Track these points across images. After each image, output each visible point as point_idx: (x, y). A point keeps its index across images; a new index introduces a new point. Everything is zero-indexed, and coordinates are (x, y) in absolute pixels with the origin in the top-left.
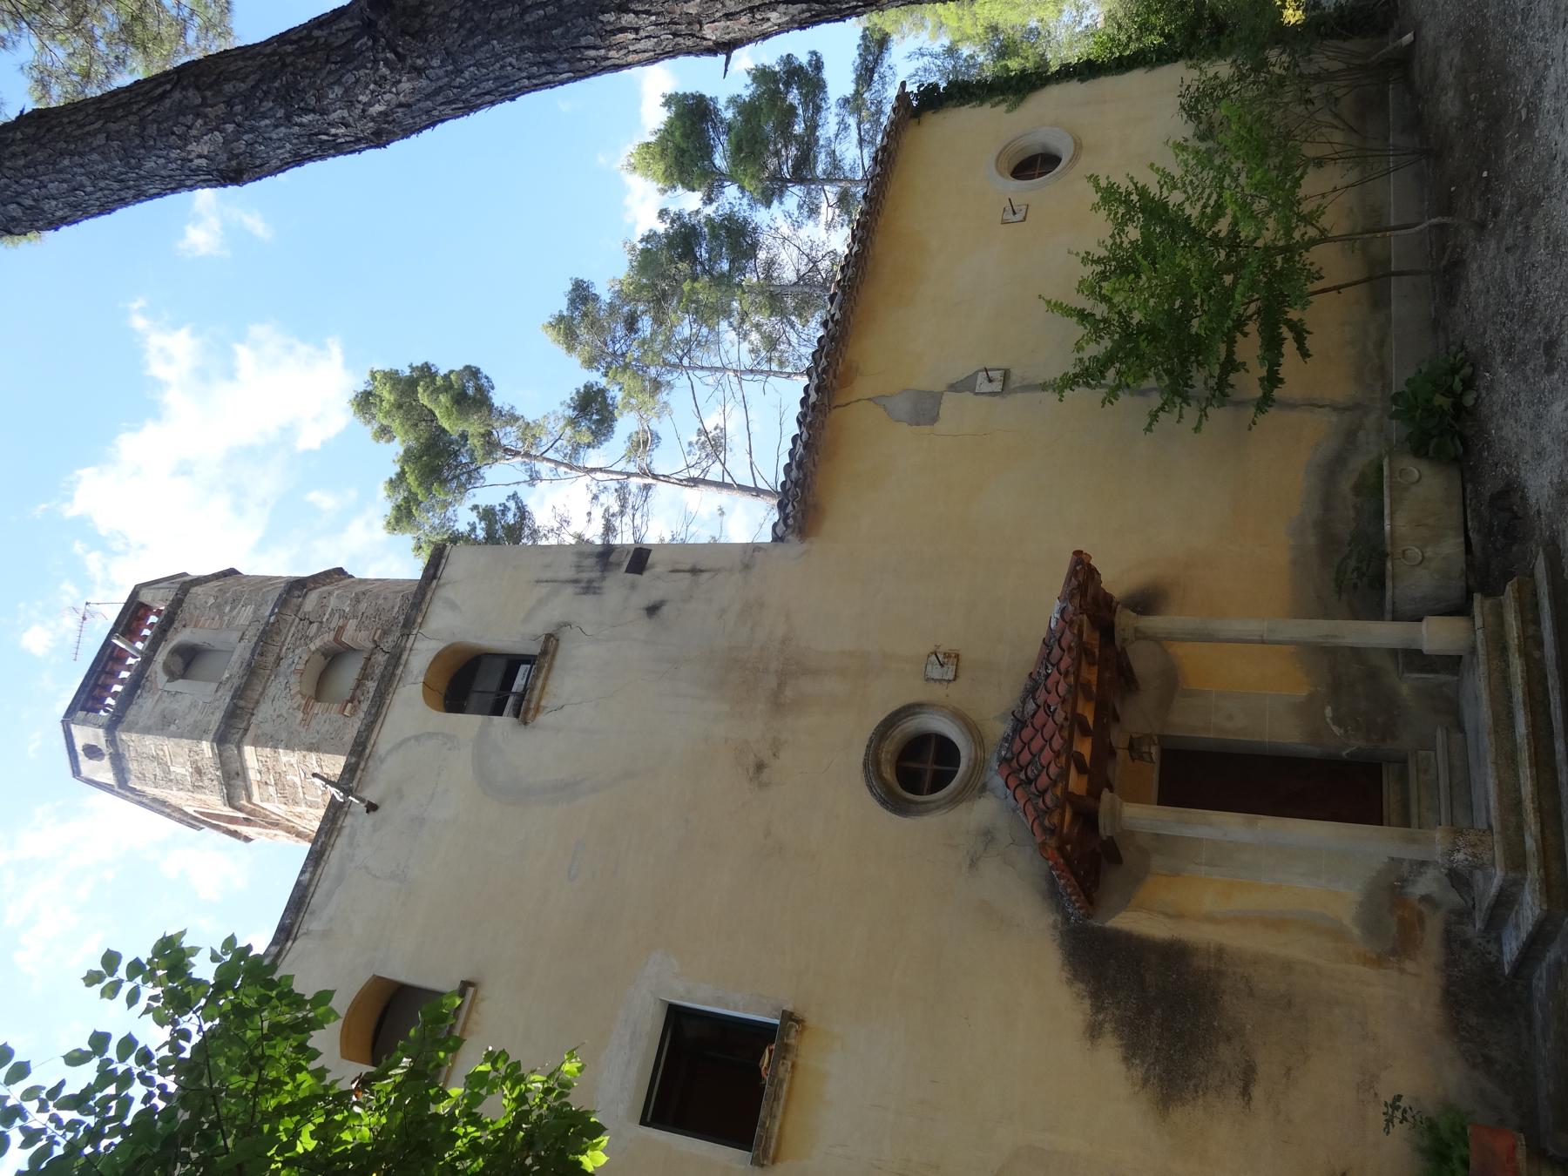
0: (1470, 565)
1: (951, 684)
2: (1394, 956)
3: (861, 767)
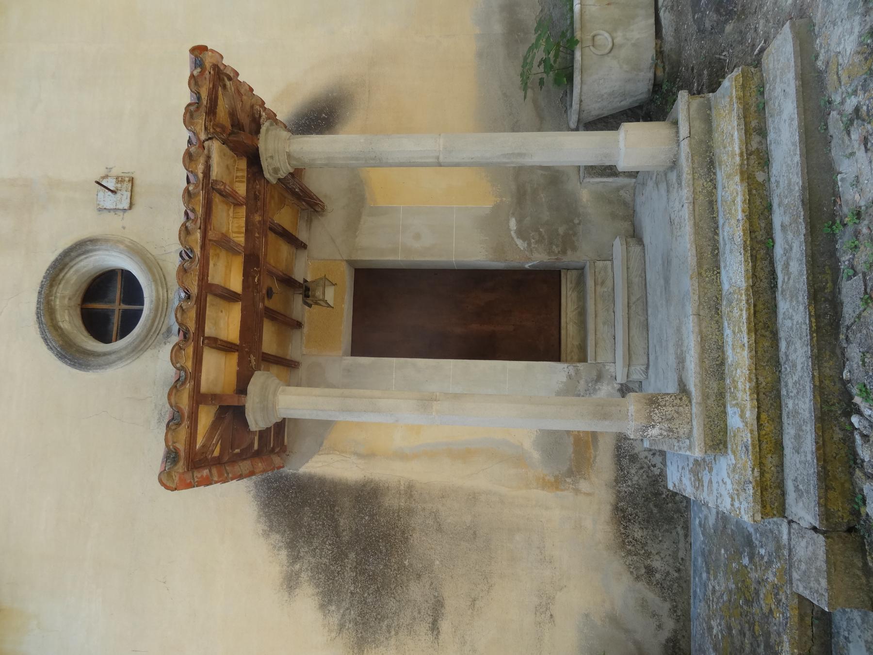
0: (660, 53)
1: (126, 214)
2: (570, 477)
3: (35, 317)
